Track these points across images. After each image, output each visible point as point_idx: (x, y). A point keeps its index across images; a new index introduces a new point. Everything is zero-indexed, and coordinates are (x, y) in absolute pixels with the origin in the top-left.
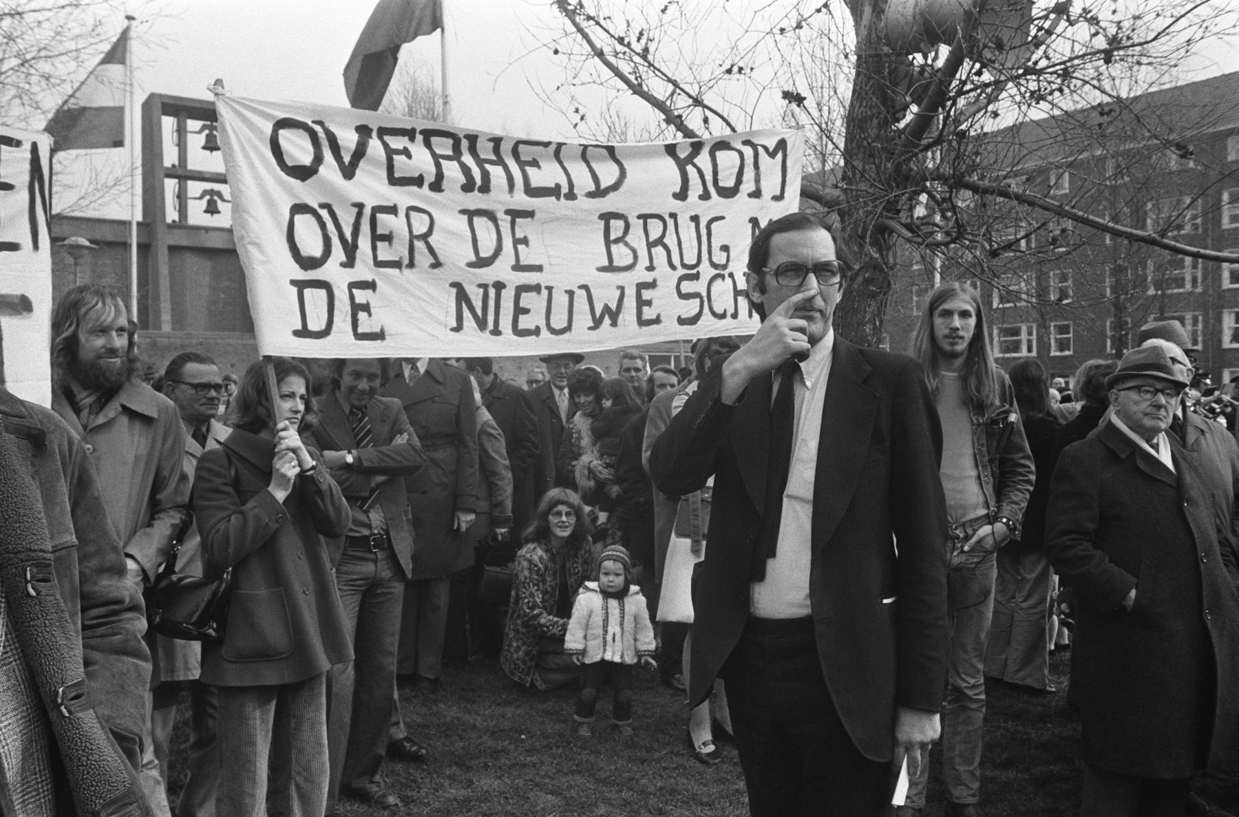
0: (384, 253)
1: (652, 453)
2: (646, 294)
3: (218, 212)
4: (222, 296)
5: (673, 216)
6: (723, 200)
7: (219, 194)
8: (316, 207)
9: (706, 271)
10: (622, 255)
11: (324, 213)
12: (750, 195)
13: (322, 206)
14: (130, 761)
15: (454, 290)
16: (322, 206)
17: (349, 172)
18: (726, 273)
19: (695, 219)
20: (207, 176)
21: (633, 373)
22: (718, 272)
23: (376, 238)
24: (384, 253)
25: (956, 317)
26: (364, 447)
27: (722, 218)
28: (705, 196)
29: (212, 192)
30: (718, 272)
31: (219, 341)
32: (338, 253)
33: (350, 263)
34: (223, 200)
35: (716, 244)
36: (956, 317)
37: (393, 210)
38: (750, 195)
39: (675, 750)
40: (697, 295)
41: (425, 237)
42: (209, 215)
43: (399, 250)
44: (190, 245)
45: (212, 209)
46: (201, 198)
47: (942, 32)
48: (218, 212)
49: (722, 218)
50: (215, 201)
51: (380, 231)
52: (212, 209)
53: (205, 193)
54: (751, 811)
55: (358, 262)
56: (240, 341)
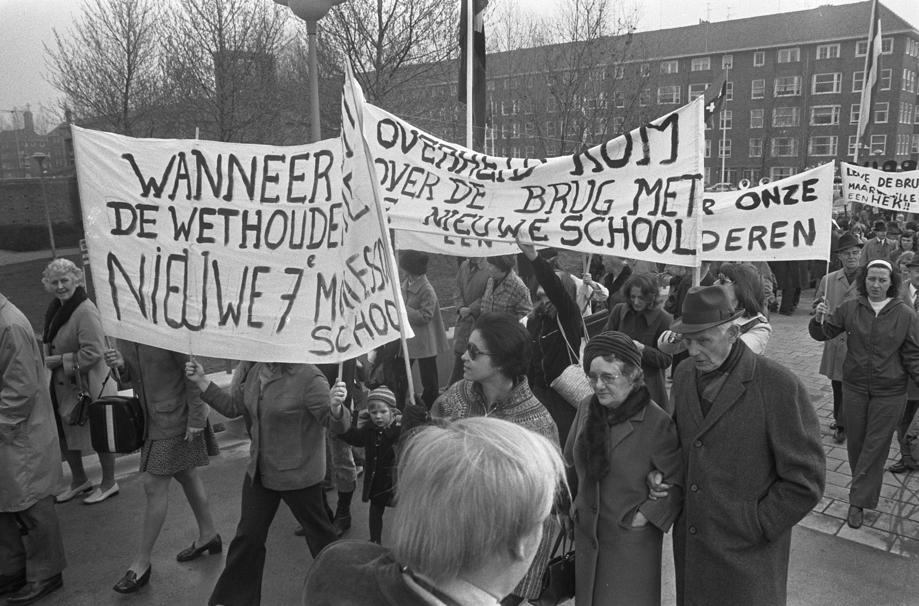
0: (409, 188)
5: (576, 182)
6: (612, 169)
8: (388, 161)
9: (588, 215)
10: (535, 204)
11: (390, 165)
12: (638, 163)
13: (391, 162)
14: (4, 370)
15: (433, 211)
16: (391, 162)
17: (406, 149)
18: (607, 217)
19: (592, 183)
22: (599, 216)
23: (409, 181)
24: (409, 188)
25: (877, 281)
26: (174, 158)
27: (613, 181)
28: (599, 169)
32: (388, 184)
33: (390, 190)
35: (603, 198)
36: (877, 281)
37: (422, 171)
38: (638, 163)
40: (576, 228)
41: (430, 186)
43: (415, 189)
47: (865, 52)
49: (613, 181)
51: (411, 179)
54: (882, 480)
55: (394, 190)
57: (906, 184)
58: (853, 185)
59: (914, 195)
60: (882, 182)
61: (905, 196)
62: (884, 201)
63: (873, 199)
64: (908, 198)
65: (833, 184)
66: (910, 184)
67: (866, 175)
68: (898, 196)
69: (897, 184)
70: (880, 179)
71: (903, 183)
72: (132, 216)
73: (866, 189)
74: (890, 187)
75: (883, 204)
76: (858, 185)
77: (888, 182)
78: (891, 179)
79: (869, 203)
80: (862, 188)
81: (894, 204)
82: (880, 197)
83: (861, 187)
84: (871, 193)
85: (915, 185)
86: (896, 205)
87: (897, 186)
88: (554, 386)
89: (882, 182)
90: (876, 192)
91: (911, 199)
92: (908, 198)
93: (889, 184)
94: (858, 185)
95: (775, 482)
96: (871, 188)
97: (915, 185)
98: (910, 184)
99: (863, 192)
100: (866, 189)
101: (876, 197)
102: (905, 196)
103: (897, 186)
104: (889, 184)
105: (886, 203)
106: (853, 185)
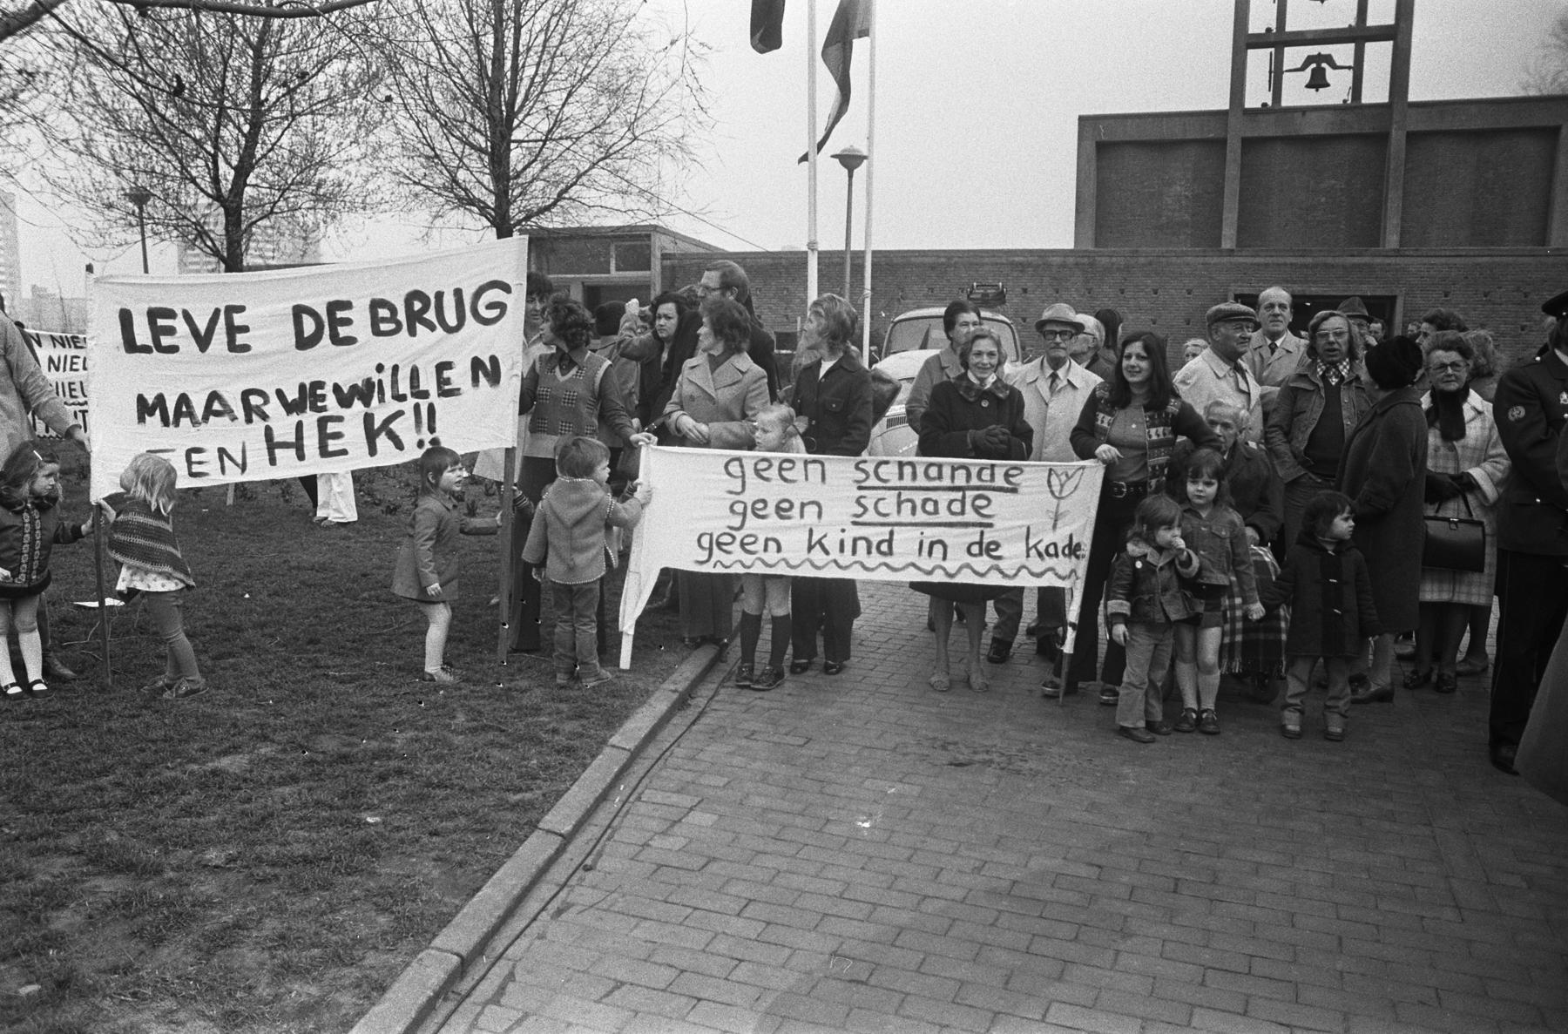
1: (1198, 417)
2: (238, 319)
3: (1328, 85)
4: (1323, 200)
7: (1329, 59)
20: (1310, 37)
21: (1450, 371)
25: (985, 356)
29: (1319, 58)
30: (325, 318)
31: (1174, 260)
34: (1334, 67)
36: (985, 356)
39: (106, 226)
42: (1313, 90)
44: (1279, 134)
45: (1318, 82)
46: (1303, 69)
48: (1328, 85)
50: (1324, 69)
52: (1318, 82)
53: (1310, 60)
56: (1201, 260)
57: (415, 318)
58: (160, 399)
59: (447, 365)
60: (309, 326)
61: (415, 374)
62: (324, 437)
63: (272, 445)
64: (428, 382)
65: (90, 407)
66: (431, 315)
67: (231, 310)
68: (386, 377)
69: (375, 321)
70: (299, 311)
71: (402, 316)
72: (496, 290)
73: (227, 411)
74: (350, 341)
75: (324, 452)
76: (183, 399)
77: (335, 323)
78: (347, 305)
79: (260, 471)
80: (209, 412)
81: (371, 436)
82: (299, 426)
83: (199, 411)
84: (258, 425)
85: (452, 320)
86: (383, 442)
87: (377, 332)
88: (1497, 484)
89: (309, 326)
90: (274, 408)
91: (442, 382)
92: (428, 382)
93: (343, 331)
94: (183, 399)
95: (1281, 428)
96: (246, 395)
97: (452, 320)
98: (431, 315)
99: (216, 434)
100: (227, 411)
101: (284, 427)
102: (415, 374)
103: (377, 332)
104: (343, 331)
105: (333, 445)
106: (160, 399)
